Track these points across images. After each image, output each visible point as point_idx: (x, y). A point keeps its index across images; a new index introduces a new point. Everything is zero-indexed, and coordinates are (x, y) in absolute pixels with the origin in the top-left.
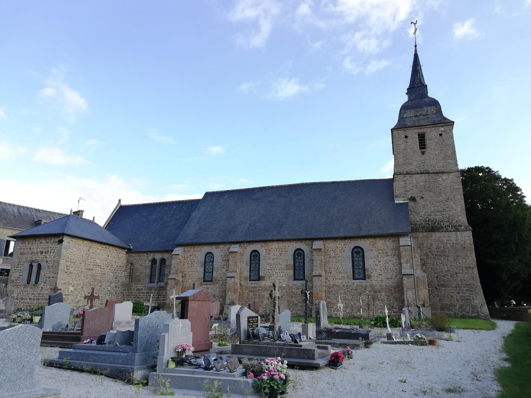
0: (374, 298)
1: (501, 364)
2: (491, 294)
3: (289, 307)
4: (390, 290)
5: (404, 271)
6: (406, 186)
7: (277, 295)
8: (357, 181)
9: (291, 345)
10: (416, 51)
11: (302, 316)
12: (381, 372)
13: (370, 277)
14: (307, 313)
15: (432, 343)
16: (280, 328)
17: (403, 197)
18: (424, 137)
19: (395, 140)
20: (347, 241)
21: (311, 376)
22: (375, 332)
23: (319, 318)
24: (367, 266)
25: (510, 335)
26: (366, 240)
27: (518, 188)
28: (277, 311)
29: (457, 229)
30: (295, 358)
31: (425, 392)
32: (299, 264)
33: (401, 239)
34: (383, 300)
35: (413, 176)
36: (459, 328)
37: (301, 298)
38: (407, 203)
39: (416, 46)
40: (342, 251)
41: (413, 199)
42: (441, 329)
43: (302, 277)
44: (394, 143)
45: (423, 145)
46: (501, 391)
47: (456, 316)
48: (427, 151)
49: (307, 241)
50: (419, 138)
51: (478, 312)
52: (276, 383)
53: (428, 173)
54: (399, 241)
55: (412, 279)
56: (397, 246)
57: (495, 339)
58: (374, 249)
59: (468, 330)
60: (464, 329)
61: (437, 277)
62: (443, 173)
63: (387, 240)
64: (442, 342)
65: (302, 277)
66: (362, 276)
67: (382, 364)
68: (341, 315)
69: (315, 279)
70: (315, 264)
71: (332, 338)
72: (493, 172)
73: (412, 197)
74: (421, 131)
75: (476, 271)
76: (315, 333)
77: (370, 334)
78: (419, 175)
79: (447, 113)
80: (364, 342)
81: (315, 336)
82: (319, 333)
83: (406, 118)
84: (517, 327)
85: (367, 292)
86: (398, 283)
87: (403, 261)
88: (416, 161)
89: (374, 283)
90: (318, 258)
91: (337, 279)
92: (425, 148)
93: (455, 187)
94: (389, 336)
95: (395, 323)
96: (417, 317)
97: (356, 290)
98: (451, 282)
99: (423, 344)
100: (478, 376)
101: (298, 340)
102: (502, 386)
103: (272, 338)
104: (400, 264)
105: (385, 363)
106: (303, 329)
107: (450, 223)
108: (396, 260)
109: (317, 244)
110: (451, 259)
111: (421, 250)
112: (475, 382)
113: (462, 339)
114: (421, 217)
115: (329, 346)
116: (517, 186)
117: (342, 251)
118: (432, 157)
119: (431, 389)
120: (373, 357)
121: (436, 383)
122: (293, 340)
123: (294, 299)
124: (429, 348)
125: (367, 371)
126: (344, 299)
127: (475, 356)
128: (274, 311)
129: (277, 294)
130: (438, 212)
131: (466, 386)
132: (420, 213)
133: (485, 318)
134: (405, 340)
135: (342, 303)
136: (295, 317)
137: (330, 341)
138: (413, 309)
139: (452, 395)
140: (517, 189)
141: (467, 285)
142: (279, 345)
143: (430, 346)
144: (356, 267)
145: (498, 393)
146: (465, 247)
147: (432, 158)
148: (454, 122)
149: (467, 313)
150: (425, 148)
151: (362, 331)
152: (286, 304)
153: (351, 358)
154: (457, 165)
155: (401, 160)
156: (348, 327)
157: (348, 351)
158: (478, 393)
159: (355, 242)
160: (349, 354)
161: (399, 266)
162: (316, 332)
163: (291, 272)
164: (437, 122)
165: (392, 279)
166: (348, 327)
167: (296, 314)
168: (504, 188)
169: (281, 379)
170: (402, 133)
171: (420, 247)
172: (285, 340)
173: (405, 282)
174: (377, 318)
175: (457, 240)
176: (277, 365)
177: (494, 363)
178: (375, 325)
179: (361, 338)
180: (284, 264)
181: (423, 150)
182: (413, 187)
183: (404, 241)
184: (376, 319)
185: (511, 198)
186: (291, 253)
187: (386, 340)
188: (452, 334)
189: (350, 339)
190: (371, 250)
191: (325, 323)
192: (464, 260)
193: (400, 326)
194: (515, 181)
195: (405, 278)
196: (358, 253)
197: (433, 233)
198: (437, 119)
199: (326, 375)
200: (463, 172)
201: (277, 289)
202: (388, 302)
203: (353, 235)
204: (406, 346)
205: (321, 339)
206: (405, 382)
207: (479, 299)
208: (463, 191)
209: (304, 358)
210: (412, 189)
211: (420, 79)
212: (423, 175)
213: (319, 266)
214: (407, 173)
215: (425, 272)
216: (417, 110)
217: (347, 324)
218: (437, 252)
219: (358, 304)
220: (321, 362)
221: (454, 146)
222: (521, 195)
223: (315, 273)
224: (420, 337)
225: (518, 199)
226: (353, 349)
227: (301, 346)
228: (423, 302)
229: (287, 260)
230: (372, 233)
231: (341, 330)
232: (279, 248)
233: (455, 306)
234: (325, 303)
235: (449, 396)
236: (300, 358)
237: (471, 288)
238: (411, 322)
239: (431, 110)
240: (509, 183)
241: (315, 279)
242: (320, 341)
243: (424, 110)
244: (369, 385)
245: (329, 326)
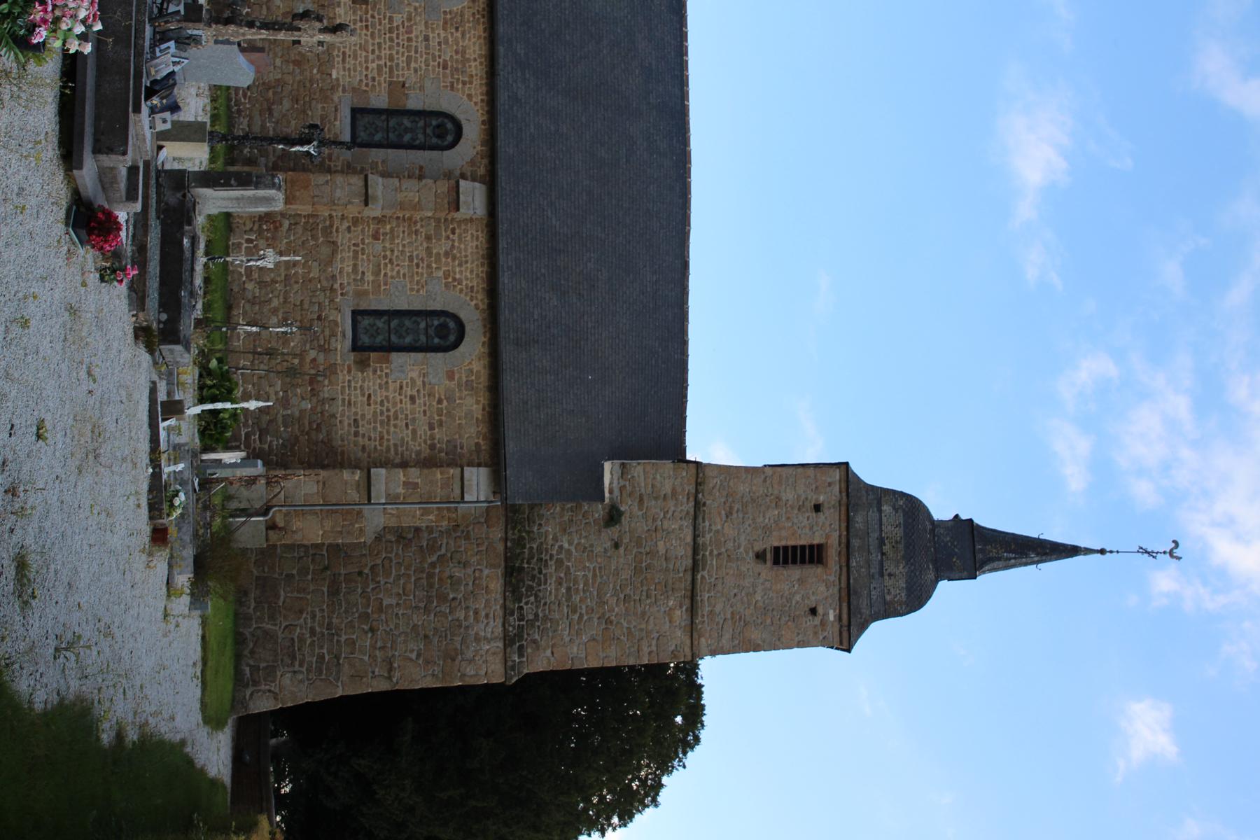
0: (292, 372)
1: (106, 725)
2: (310, 724)
3: (261, 85)
4: (319, 429)
5: (379, 474)
6: (656, 498)
7: (304, 39)
8: (685, 343)
9: (138, 75)
10: (1088, 551)
11: (231, 125)
12: (64, 367)
13: (363, 365)
14: (241, 147)
15: (159, 536)
16: (196, 40)
17: (622, 489)
18: (811, 561)
19: (811, 471)
20: (481, 298)
21: (42, 137)
22: (185, 364)
23: (227, 185)
24: (398, 358)
25: (190, 762)
26: (485, 361)
27: (631, 817)
28: (251, 35)
29: (512, 642)
30: (98, 86)
31: (12, 491)
32: (407, 130)
33: (483, 471)
34: (285, 403)
35: (687, 523)
36: (204, 623)
37: (293, 127)
38: (602, 499)
39: (1102, 552)
40: (445, 275)
41: (613, 517)
42: (200, 566)
43: (363, 136)
44: (800, 470)
45: (786, 556)
46: (31, 709)
47: (240, 619)
48: (766, 571)
49: (485, 161)
50: (811, 547)
51: (256, 683)
52: (17, 10)
53: (695, 568)
54: (479, 465)
55: (354, 495)
56: (461, 456)
57: (178, 718)
58: (453, 385)
59: (199, 649)
60: (203, 637)
61: (360, 573)
62: (692, 611)
63: (483, 428)
64: (161, 567)
65: (363, 136)
66: (365, 339)
67: (89, 373)
68: (237, 260)
69: (357, 181)
70: (407, 184)
71: (163, 224)
72: (685, 753)
73: (620, 514)
74: (832, 555)
75: (383, 686)
76: (176, 166)
77: (178, 348)
78: (689, 539)
79: (878, 632)
80: (155, 325)
81: (167, 167)
82: (179, 180)
83: (880, 511)
84: (215, 783)
85: (313, 354)
86: (343, 453)
87: (414, 474)
88: (736, 535)
89: (343, 376)
90: (427, 194)
91: (355, 257)
92: (776, 562)
93: (644, 644)
94: (173, 408)
95: (214, 431)
96: (234, 505)
97: (319, 318)
98: (346, 612)
99: (155, 509)
100: (68, 654)
101: (155, 101)
102: (45, 713)
103: (160, 10)
104: (404, 465)
105: (92, 386)
106: (189, 124)
107: (531, 623)
108: (418, 453)
109: (473, 197)
110: (417, 619)
111: (448, 533)
112: (53, 643)
113: (172, 627)
114: (555, 539)
115: (138, 207)
116: (637, 817)
117: (445, 275)
118: (747, 583)
119: (21, 513)
120: (108, 348)
121: (41, 529)
122: (154, 82)
123: (286, 104)
124: (143, 525)
125: (64, 325)
126: (286, 274)
127: (125, 654)
128: (251, 25)
129: (310, 37)
130: (569, 589)
131: (37, 616)
132: (564, 535)
133: (237, 702)
134: (164, 457)
135: (277, 264)
136: (229, 107)
137: (152, 213)
138: (259, 492)
139: (10, 572)
140: (626, 817)
141: (337, 657)
142: (140, 32)
143: (147, 530)
144: (394, 323)
145: (25, 697)
146: (453, 660)
147: (739, 581)
148: (849, 651)
149: (252, 652)
150: (776, 562)
151: (187, 326)
152: (273, 76)
153: (102, 279)
154: (714, 653)
155: (743, 488)
156: (198, 281)
157: (124, 270)
158: (22, 646)
159: (480, 324)
160: (114, 271)
161: (397, 461)
162: (182, 173)
163: (380, 100)
164: (854, 602)
165: (356, 434)
166: (198, 281)
167: (239, 111)
168: (632, 780)
169: (31, 28)
170: (830, 496)
171: (458, 529)
172: (154, 57)
173: (346, 474)
174: (229, 380)
175: (477, 639)
176: (74, 17)
177: (107, 704)
178: (205, 372)
179: (164, 317)
180: (411, 78)
181: (769, 556)
182: (654, 520)
183: (478, 482)
184: (225, 376)
185: (602, 798)
186: (446, 105)
187: (162, 396)
188: (186, 599)
189: (163, 283)
190: (450, 376)
191: (213, 202)
192: (414, 656)
193: (206, 449)
194: (650, 811)
195: (358, 475)
196: (441, 332)
197: (500, 571)
198: (864, 603)
199: (45, 188)
200: (691, 669)
201: (327, 38)
202: (280, 420)
203: (502, 319)
204: (144, 458)
205: (158, 185)
206: (39, 436)
207: (292, 688)
208: (631, 668)
209: (97, 118)
210: (645, 516)
211: (999, 559)
212: (690, 553)
213: (400, 197)
214: (698, 505)
215: (378, 538)
216: (901, 546)
217: (207, 280)
218: (440, 579)
219: (274, 320)
220: (87, 174)
221: (775, 648)
222: (610, 825)
223: (378, 185)
224: (177, 502)
225: (598, 815)
226: (131, 288)
227: (137, 110)
228: (281, 525)
229: (422, 88)
230: (509, 382)
231: (188, 254)
232: (465, 61)
233: (272, 618)
234: (279, 206)
235: (6, 563)
236: (98, 104)
237: (328, 669)
238: (219, 481)
239: (896, 588)
240: (647, 795)
241: (357, 181)
242: (153, 182)
243: (897, 566)
244: (25, 324)
245: (200, 220)
